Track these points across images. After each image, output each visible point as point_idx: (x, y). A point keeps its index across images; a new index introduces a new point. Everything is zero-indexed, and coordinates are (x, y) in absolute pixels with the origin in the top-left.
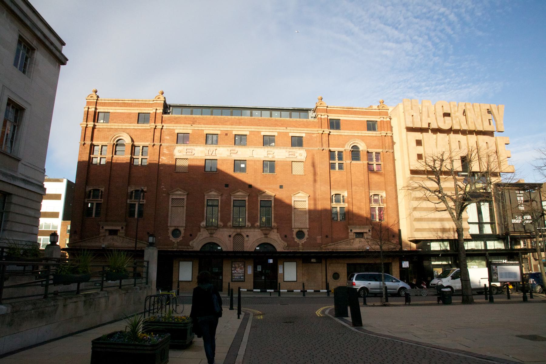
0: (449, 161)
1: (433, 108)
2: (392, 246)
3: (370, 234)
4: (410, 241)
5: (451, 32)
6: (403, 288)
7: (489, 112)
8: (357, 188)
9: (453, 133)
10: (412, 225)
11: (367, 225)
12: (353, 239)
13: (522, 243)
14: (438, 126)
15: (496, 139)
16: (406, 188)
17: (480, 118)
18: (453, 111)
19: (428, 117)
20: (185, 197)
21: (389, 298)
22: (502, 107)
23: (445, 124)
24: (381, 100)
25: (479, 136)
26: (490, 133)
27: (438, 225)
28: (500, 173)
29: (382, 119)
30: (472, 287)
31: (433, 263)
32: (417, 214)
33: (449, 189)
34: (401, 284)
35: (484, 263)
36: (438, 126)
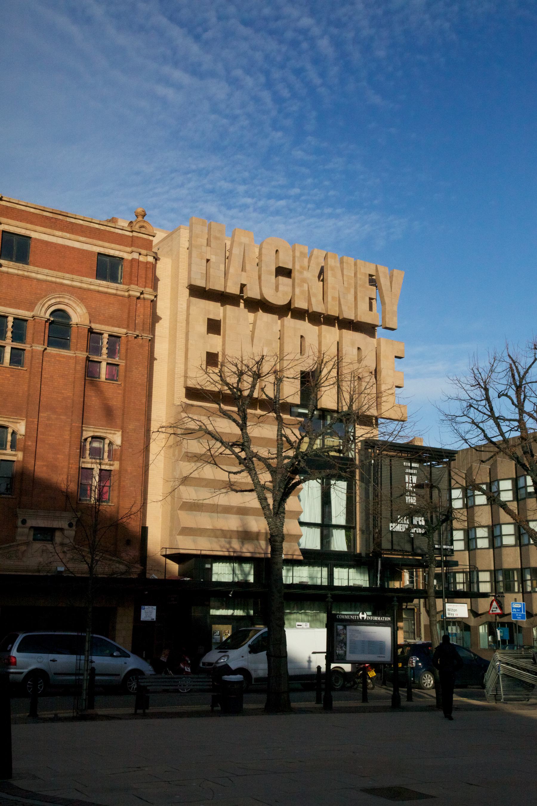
0: (272, 378)
1: (257, 250)
2: (122, 568)
3: (73, 533)
4: (167, 556)
5: (318, 81)
6: (136, 673)
7: (373, 281)
8: (54, 416)
9: (292, 317)
10: (174, 519)
11: (65, 510)
12: (27, 544)
13: (406, 576)
14: (262, 294)
15: (379, 344)
16: (171, 431)
17: (352, 291)
18: (297, 267)
19: (243, 269)
21: (99, 699)
22: (399, 275)
23: (277, 292)
24: (140, 210)
25: (344, 331)
26: (369, 329)
27: (233, 523)
28: (377, 419)
29: (135, 256)
30: (291, 672)
31: (213, 612)
32: (189, 494)
33: (264, 442)
34: (133, 662)
35: (324, 616)
36: (262, 294)
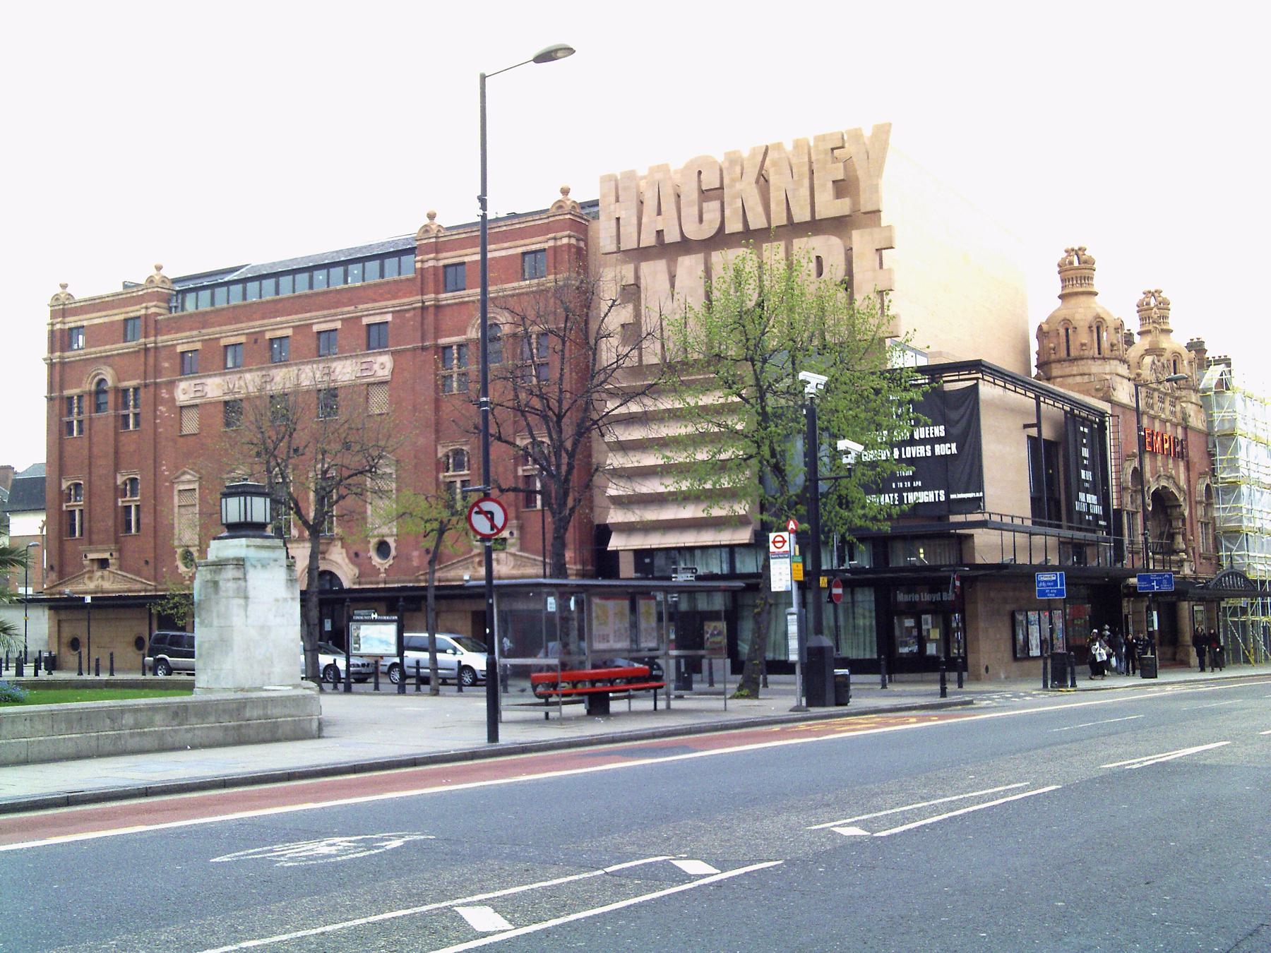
17: (806, 182)
20: (196, 486)
